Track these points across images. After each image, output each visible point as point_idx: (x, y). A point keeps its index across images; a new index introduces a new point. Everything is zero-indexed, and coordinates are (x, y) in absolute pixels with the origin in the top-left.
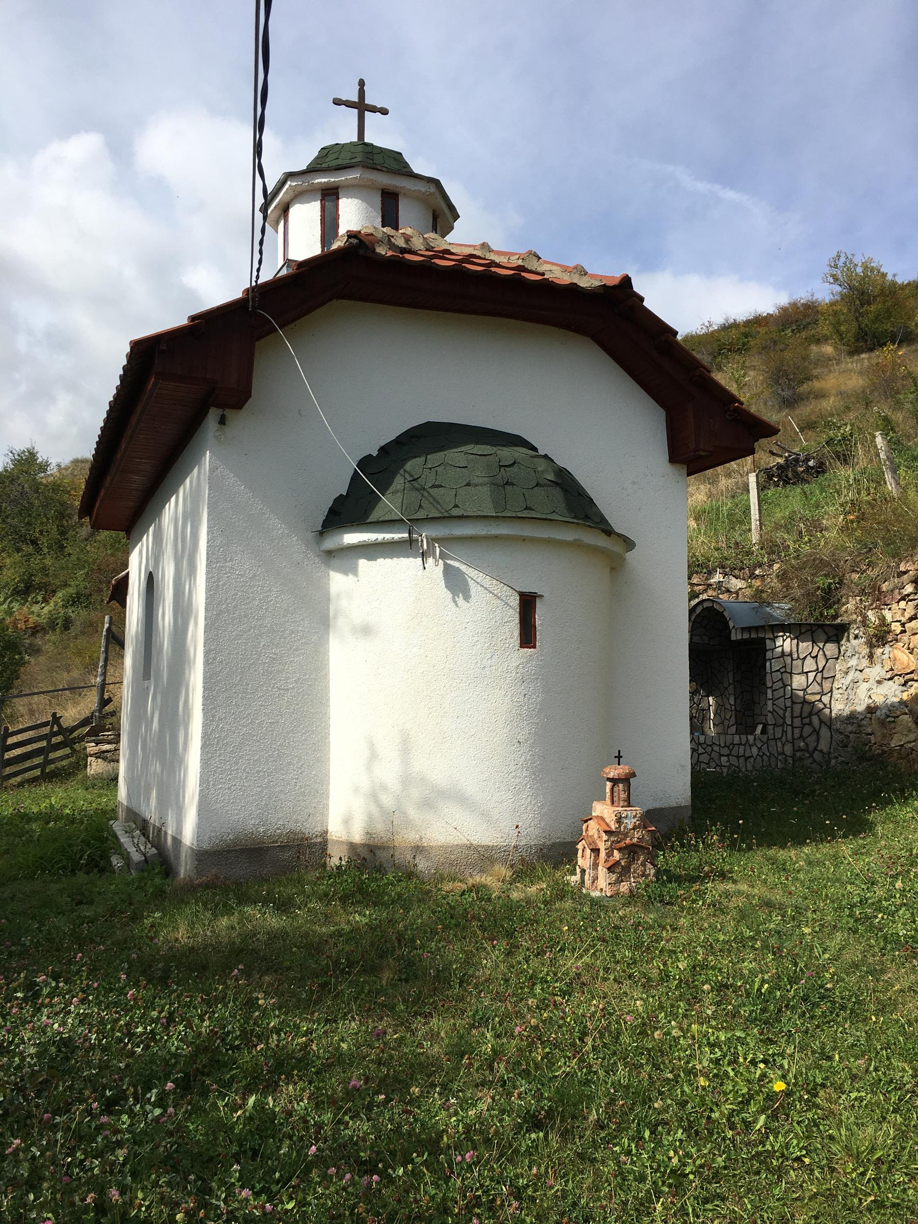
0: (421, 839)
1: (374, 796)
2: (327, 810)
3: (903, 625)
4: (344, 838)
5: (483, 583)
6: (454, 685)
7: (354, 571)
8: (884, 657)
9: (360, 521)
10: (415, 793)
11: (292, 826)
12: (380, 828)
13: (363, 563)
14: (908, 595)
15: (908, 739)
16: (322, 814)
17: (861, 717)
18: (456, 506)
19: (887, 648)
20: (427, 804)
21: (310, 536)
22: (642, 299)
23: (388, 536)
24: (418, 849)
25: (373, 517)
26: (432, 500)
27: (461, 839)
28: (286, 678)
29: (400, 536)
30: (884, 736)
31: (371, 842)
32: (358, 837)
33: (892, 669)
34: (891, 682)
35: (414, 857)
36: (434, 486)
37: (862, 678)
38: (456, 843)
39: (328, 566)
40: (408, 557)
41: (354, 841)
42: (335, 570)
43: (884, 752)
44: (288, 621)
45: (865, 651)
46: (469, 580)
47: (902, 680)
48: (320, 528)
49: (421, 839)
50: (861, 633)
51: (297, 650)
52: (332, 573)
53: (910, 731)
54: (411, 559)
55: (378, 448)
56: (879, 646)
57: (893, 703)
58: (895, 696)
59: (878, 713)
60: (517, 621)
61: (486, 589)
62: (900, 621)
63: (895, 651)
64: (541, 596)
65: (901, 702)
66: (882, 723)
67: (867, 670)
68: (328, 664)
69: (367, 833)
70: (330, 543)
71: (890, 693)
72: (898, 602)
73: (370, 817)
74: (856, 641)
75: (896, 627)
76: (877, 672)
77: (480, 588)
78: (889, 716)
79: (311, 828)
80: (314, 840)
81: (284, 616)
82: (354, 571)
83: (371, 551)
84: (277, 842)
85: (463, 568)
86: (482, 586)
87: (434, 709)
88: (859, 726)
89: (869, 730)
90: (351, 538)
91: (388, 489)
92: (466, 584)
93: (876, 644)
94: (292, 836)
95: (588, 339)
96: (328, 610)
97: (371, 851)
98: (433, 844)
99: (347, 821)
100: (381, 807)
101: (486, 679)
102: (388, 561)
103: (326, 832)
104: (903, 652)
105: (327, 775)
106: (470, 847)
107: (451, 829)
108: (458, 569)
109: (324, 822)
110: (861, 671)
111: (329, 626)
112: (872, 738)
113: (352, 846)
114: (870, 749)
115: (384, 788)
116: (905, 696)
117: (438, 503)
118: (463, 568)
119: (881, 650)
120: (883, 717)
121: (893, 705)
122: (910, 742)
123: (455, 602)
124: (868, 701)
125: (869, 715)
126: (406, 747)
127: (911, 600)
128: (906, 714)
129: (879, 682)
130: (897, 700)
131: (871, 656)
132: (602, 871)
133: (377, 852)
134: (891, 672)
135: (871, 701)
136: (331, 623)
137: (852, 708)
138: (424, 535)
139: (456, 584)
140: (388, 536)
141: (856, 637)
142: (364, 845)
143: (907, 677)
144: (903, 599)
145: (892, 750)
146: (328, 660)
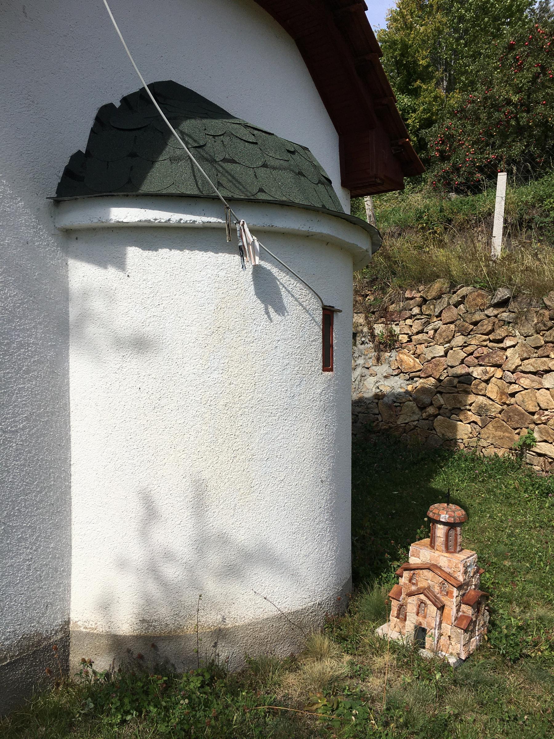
0: (224, 619)
1: (153, 570)
2: (69, 591)
3: (410, 337)
4: (101, 628)
5: (294, 292)
6: (263, 420)
7: (120, 263)
8: (391, 359)
9: (129, 190)
10: (214, 559)
11: (28, 629)
12: (164, 613)
13: (134, 254)
14: (415, 316)
15: (412, 419)
16: (62, 600)
17: (368, 402)
18: (261, 190)
19: (394, 353)
20: (232, 571)
21: (43, 202)
22: (366, 9)
23: (187, 218)
24: (220, 634)
25: (145, 188)
26: (229, 177)
27: (270, 611)
28: (15, 415)
29: (206, 219)
30: (391, 416)
31: (150, 632)
32: (125, 624)
33: (398, 368)
34: (396, 378)
35: (215, 645)
36: (225, 160)
37: (369, 373)
38: (265, 617)
39: (68, 252)
40: (206, 250)
41: (121, 633)
42: (78, 257)
43: (390, 428)
44: (15, 329)
45: (373, 354)
46: (281, 287)
47: (407, 377)
48: (54, 195)
49: (224, 619)
50: (367, 340)
51: (27, 372)
52: (72, 262)
53: (414, 413)
54: (210, 254)
55: (100, 105)
56: (386, 351)
57: (400, 393)
58: (401, 388)
59: (385, 399)
60: (321, 340)
61: (296, 300)
62: (407, 334)
63: (401, 355)
64: (340, 311)
65: (407, 392)
66: (389, 407)
67: (374, 368)
68: (68, 390)
69: (143, 621)
70: (81, 216)
71: (398, 385)
72: (405, 320)
73: (148, 601)
74: (363, 346)
75: (404, 338)
76: (384, 369)
77: (291, 299)
78: (395, 402)
79: (48, 624)
80: (55, 638)
81: (10, 321)
82: (120, 263)
83: (149, 236)
84: (6, 658)
85: (275, 271)
86: (293, 296)
87: (240, 452)
88: (368, 408)
89: (376, 411)
90: (124, 214)
91: (160, 153)
92: (278, 293)
93: (384, 349)
94: (25, 643)
95: (293, 41)
96: (67, 313)
97: (153, 646)
98: (240, 623)
99: (105, 606)
100: (164, 584)
101: (296, 409)
102: (176, 253)
103: (68, 623)
104: (409, 356)
105: (69, 546)
106: (282, 617)
107: (259, 600)
108: (269, 273)
109: (66, 610)
110: (368, 368)
111: (68, 336)
112: (379, 417)
113: (117, 643)
114: (377, 425)
115: (169, 556)
116: (410, 388)
117: (241, 185)
118: (275, 271)
119: (389, 354)
120: (390, 402)
121: (399, 394)
122: (414, 421)
123: (267, 313)
124: (374, 391)
125: (376, 401)
126: (199, 501)
127: (418, 319)
128: (410, 401)
129: (386, 377)
130: (402, 390)
131: (378, 359)
132: (447, 628)
133: (161, 645)
134: (397, 371)
135: (378, 390)
136: (72, 332)
137: (360, 395)
138: (245, 223)
139: (266, 289)
140: (187, 218)
141: (363, 343)
142: (137, 638)
143: (411, 375)
144: (410, 318)
145: (398, 427)
146: (68, 384)
